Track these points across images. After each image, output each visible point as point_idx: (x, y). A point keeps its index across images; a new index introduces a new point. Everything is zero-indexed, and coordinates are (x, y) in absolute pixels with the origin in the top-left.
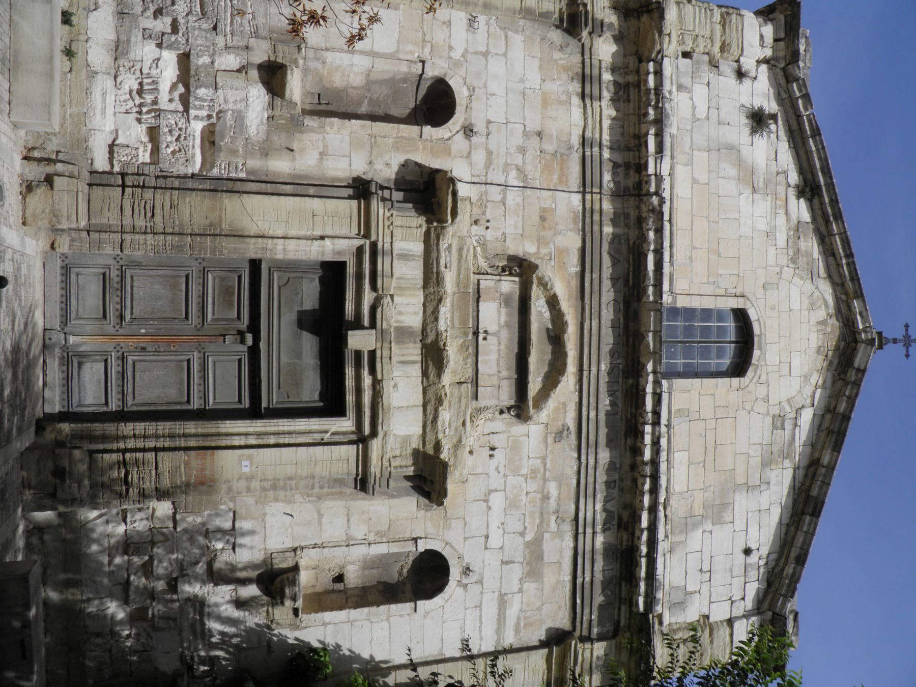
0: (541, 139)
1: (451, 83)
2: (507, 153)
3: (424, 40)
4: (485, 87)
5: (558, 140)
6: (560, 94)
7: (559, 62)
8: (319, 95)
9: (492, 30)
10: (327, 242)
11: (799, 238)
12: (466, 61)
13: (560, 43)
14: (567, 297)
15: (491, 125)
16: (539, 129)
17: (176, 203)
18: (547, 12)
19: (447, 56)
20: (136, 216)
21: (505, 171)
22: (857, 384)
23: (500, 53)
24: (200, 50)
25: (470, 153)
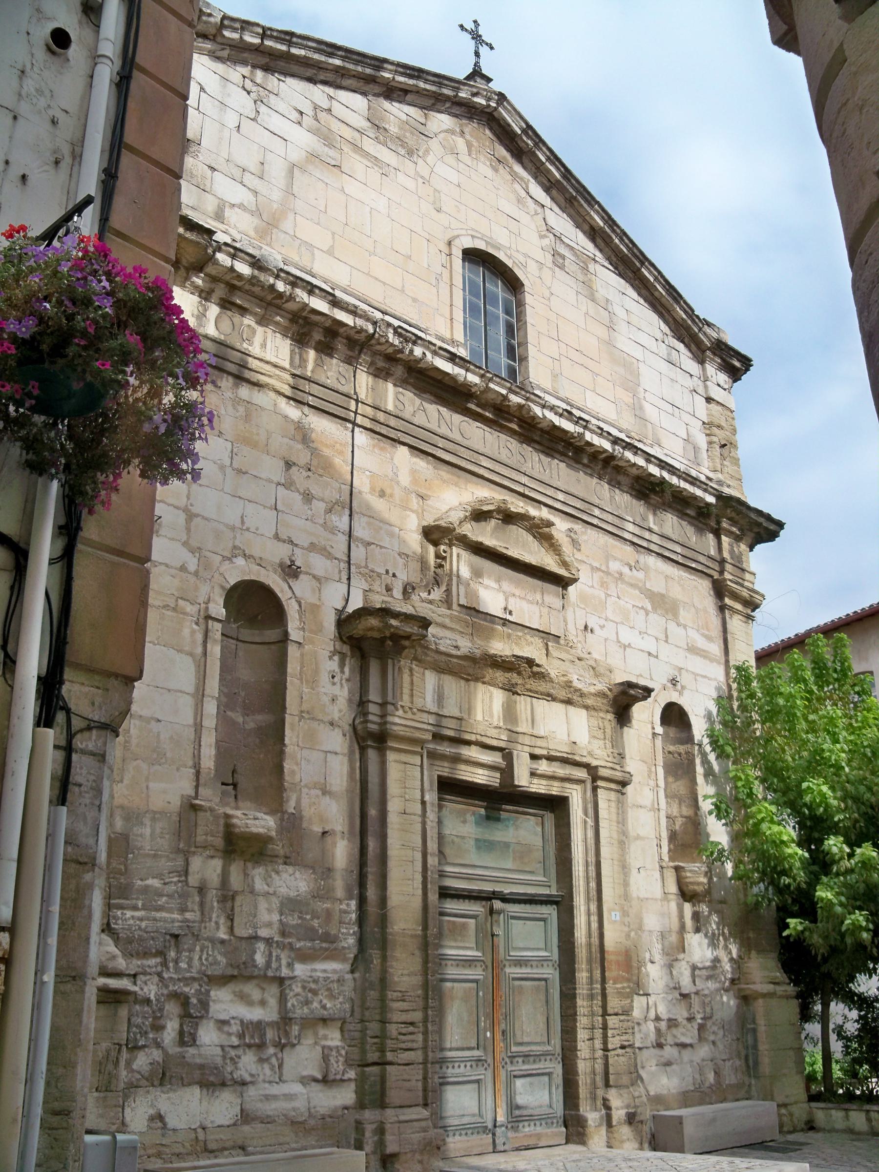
0: (294, 464)
1: (232, 582)
3: (174, 609)
4: (233, 528)
8: (223, 784)
10: (427, 798)
11: (385, 129)
14: (457, 489)
16: (282, 463)
17: (400, 994)
20: (415, 1045)
21: (333, 530)
22: (539, 141)
23: (186, 492)
24: (206, 959)
25: (314, 577)
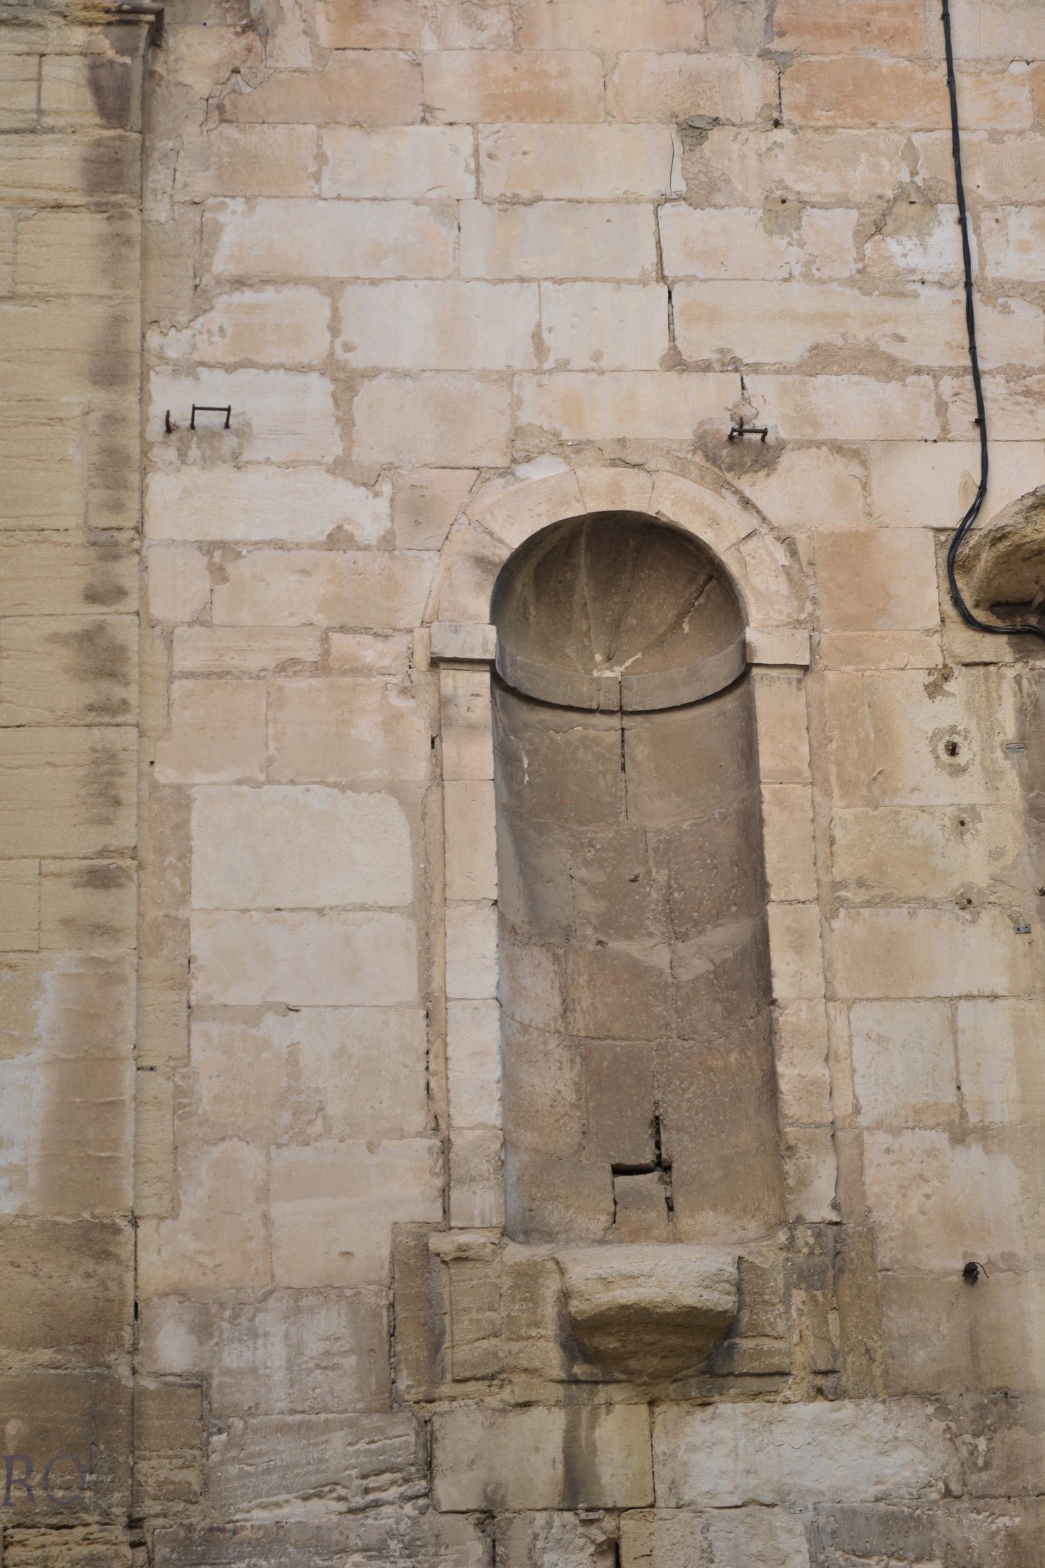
0: (716, 121)
1: (516, 537)
2: (808, 277)
3: (321, 667)
4: (506, 378)
5: (703, 47)
6: (483, 37)
7: (325, 39)
8: (619, 1170)
9: (216, 350)
12: (391, 467)
13: (229, 34)
15: (688, 353)
16: (669, 135)
18: (96, 87)
19: (383, 559)
23: (327, 313)
25: (838, 448)
